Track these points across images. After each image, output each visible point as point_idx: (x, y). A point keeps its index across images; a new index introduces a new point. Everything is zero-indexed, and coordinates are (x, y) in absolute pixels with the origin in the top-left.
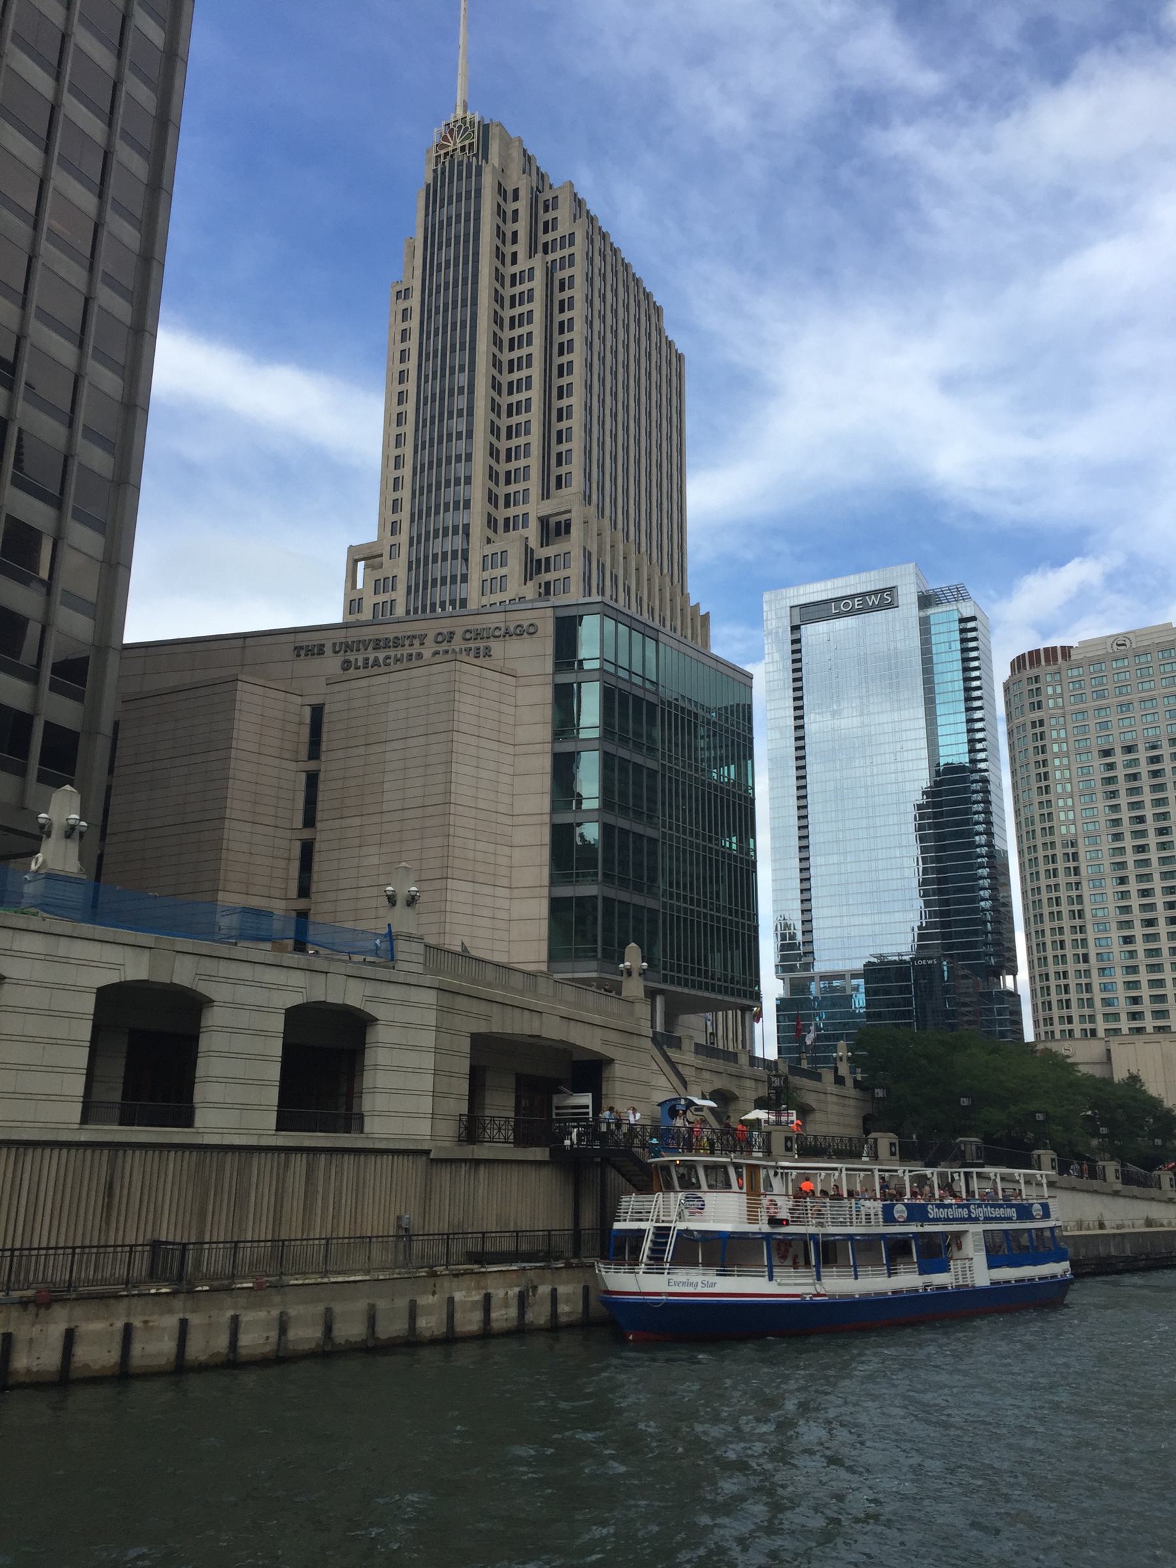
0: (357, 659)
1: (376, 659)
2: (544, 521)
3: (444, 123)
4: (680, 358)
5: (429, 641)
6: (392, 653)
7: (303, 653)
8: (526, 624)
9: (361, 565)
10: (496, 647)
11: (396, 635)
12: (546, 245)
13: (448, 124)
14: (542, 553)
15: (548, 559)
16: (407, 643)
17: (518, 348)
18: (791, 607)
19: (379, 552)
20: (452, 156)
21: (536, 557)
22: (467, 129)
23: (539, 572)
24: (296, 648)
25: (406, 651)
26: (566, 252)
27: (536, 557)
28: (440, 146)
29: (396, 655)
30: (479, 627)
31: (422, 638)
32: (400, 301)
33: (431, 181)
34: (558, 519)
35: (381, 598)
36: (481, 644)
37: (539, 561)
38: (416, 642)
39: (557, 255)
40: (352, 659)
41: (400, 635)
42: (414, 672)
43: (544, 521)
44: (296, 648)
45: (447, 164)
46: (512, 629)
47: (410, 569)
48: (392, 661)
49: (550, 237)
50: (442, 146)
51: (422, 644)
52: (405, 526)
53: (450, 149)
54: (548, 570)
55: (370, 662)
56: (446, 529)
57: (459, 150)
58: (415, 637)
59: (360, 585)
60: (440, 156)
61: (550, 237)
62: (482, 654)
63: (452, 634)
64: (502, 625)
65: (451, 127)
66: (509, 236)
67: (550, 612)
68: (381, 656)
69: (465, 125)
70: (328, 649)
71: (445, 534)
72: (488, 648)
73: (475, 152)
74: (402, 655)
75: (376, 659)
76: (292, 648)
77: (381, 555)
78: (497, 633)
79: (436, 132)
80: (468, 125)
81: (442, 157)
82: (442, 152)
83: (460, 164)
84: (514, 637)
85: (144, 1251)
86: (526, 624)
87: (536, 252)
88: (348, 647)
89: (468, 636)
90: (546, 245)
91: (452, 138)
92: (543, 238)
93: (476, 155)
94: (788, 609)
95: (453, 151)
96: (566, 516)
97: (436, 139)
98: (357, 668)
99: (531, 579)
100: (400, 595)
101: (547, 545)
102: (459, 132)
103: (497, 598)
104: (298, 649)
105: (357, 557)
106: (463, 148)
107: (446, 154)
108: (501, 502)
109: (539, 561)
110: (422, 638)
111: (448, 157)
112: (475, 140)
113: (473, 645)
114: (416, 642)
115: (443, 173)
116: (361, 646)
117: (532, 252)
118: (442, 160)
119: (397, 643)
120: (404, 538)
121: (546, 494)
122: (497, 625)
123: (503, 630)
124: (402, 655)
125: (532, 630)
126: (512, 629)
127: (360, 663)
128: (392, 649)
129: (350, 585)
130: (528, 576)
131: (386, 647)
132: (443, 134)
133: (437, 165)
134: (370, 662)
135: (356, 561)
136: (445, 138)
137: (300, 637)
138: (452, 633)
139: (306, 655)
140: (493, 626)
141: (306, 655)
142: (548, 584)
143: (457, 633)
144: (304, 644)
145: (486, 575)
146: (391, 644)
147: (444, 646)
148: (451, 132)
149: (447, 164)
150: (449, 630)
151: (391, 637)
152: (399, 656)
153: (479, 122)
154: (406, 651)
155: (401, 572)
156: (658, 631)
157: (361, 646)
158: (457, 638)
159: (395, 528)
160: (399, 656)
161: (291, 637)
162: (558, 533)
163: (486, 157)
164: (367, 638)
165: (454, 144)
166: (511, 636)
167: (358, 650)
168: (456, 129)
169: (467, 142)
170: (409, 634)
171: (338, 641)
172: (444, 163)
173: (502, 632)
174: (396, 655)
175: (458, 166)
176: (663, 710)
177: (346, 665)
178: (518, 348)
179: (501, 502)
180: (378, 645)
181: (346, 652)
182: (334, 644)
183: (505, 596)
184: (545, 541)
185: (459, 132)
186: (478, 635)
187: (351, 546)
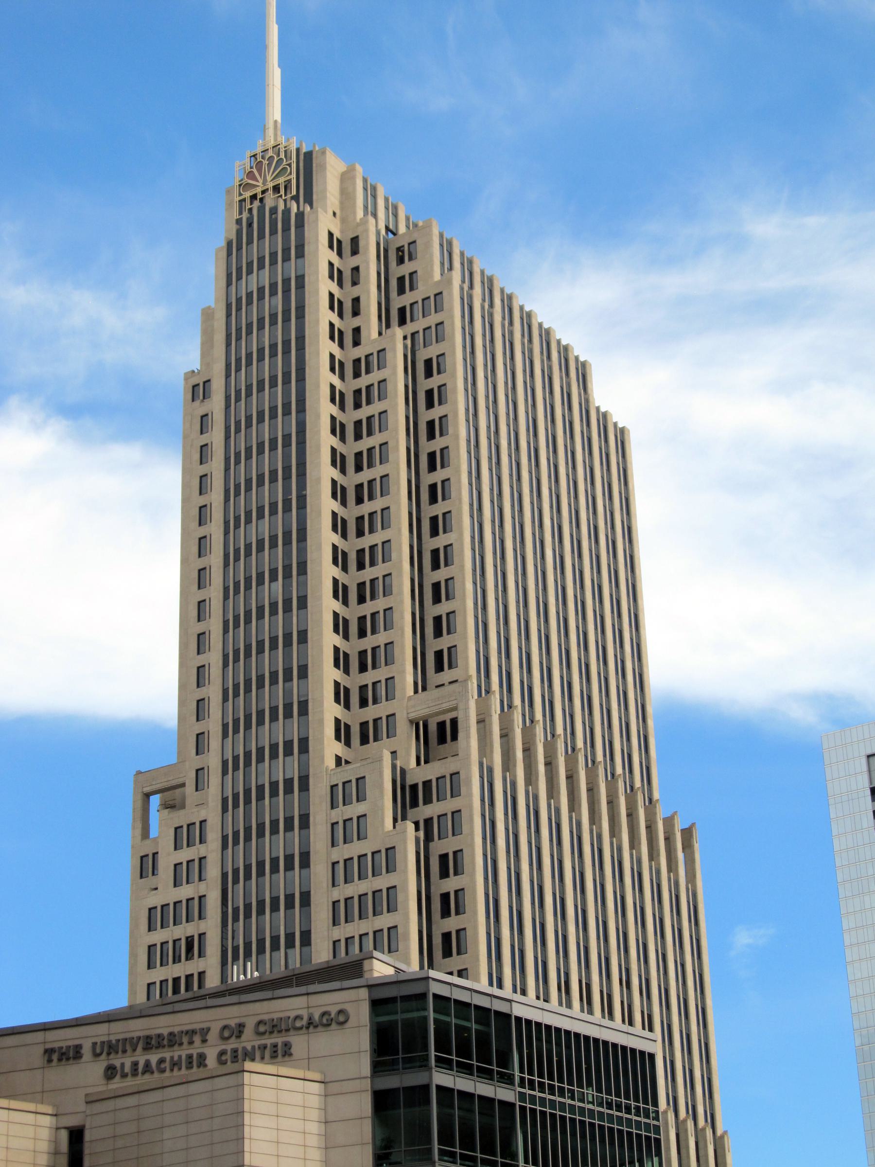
0: (123, 1065)
1: (147, 1064)
2: (420, 727)
3: (248, 154)
4: (622, 435)
5: (213, 1036)
6: (167, 1054)
7: (55, 1057)
8: (333, 1010)
9: (155, 800)
10: (298, 1042)
11: (170, 1030)
12: (402, 311)
13: (255, 156)
14: (418, 775)
15: (427, 784)
16: (185, 1040)
17: (369, 467)
18: (869, 756)
19: (180, 781)
20: (261, 200)
21: (409, 781)
22: (280, 161)
23: (414, 804)
24: (46, 1051)
25: (182, 1052)
26: (432, 319)
27: (409, 781)
30: (276, 1016)
31: (204, 1033)
33: (233, 236)
34: (441, 718)
35: (184, 855)
36: (279, 1040)
37: (414, 787)
38: (197, 1039)
39: (418, 325)
40: (117, 1063)
41: (176, 1030)
42: (194, 1087)
43: (420, 727)
44: (46, 1051)
45: (255, 212)
46: (316, 1017)
47: (225, 809)
48: (167, 1065)
49: (407, 299)
50: (247, 187)
51: (204, 1041)
53: (259, 190)
54: (428, 800)
56: (274, 747)
57: (271, 192)
59: (154, 832)
60: (244, 200)
61: (407, 299)
62: (280, 1052)
63: (241, 1026)
64: (305, 1013)
65: (259, 159)
66: (348, 306)
67: (364, 993)
68: (154, 1058)
69: (278, 155)
71: (274, 755)
72: (287, 1045)
73: (294, 192)
75: (147, 1064)
76: (42, 1051)
77: (183, 785)
78: (298, 1024)
79: (240, 165)
80: (282, 156)
81: (248, 201)
82: (247, 194)
83: (274, 211)
85: (265, 1047)
86: (333, 1010)
87: (388, 326)
88: (111, 1048)
89: (262, 1029)
90: (402, 311)
92: (397, 302)
93: (296, 198)
94: (864, 760)
95: (263, 192)
97: (238, 176)
98: (124, 1076)
99: (404, 818)
100: (212, 849)
101: (426, 762)
102: (269, 165)
103: (355, 849)
104: (49, 1052)
105: (147, 789)
106: (276, 189)
107: (254, 197)
108: (355, 699)
109: (414, 787)
110: (204, 1033)
111: (256, 203)
112: (294, 175)
113: (269, 1041)
114: (197, 1039)
115: (250, 225)
116: (128, 1047)
117: (385, 320)
118: (248, 206)
119: (173, 1040)
120: (213, 760)
121: (422, 685)
122: (299, 1012)
125: (341, 1018)
126: (316, 1017)
127: (127, 1069)
128: (166, 1049)
129: (138, 832)
130: (399, 816)
131: (160, 1046)
132: (248, 169)
133: (241, 213)
135: (147, 796)
137: (52, 1036)
139: (60, 1060)
140: (293, 1014)
141: (60, 1060)
142: (428, 822)
144: (56, 1045)
145: (339, 814)
146: (165, 1042)
147: (230, 1046)
148: (259, 165)
149: (255, 212)
150: (237, 1021)
151: (165, 1032)
152: (176, 1058)
154: (182, 1052)
155: (212, 814)
156: (510, 1001)
157: (128, 1047)
158: (248, 1032)
159: (200, 743)
160: (176, 1058)
161: (40, 1036)
162: (442, 740)
163: (309, 200)
166: (316, 1027)
167: (124, 1051)
168: (266, 162)
169: (281, 180)
170: (185, 1028)
171: (98, 1040)
172: (250, 210)
173: (304, 1022)
174: (172, 1058)
176: (523, 1109)
177: (110, 1072)
178: (369, 467)
180: (150, 1043)
181: (109, 1054)
182: (95, 1044)
183: (365, 847)
184: (425, 758)
185: (269, 165)
186: (275, 1027)
187: (139, 773)
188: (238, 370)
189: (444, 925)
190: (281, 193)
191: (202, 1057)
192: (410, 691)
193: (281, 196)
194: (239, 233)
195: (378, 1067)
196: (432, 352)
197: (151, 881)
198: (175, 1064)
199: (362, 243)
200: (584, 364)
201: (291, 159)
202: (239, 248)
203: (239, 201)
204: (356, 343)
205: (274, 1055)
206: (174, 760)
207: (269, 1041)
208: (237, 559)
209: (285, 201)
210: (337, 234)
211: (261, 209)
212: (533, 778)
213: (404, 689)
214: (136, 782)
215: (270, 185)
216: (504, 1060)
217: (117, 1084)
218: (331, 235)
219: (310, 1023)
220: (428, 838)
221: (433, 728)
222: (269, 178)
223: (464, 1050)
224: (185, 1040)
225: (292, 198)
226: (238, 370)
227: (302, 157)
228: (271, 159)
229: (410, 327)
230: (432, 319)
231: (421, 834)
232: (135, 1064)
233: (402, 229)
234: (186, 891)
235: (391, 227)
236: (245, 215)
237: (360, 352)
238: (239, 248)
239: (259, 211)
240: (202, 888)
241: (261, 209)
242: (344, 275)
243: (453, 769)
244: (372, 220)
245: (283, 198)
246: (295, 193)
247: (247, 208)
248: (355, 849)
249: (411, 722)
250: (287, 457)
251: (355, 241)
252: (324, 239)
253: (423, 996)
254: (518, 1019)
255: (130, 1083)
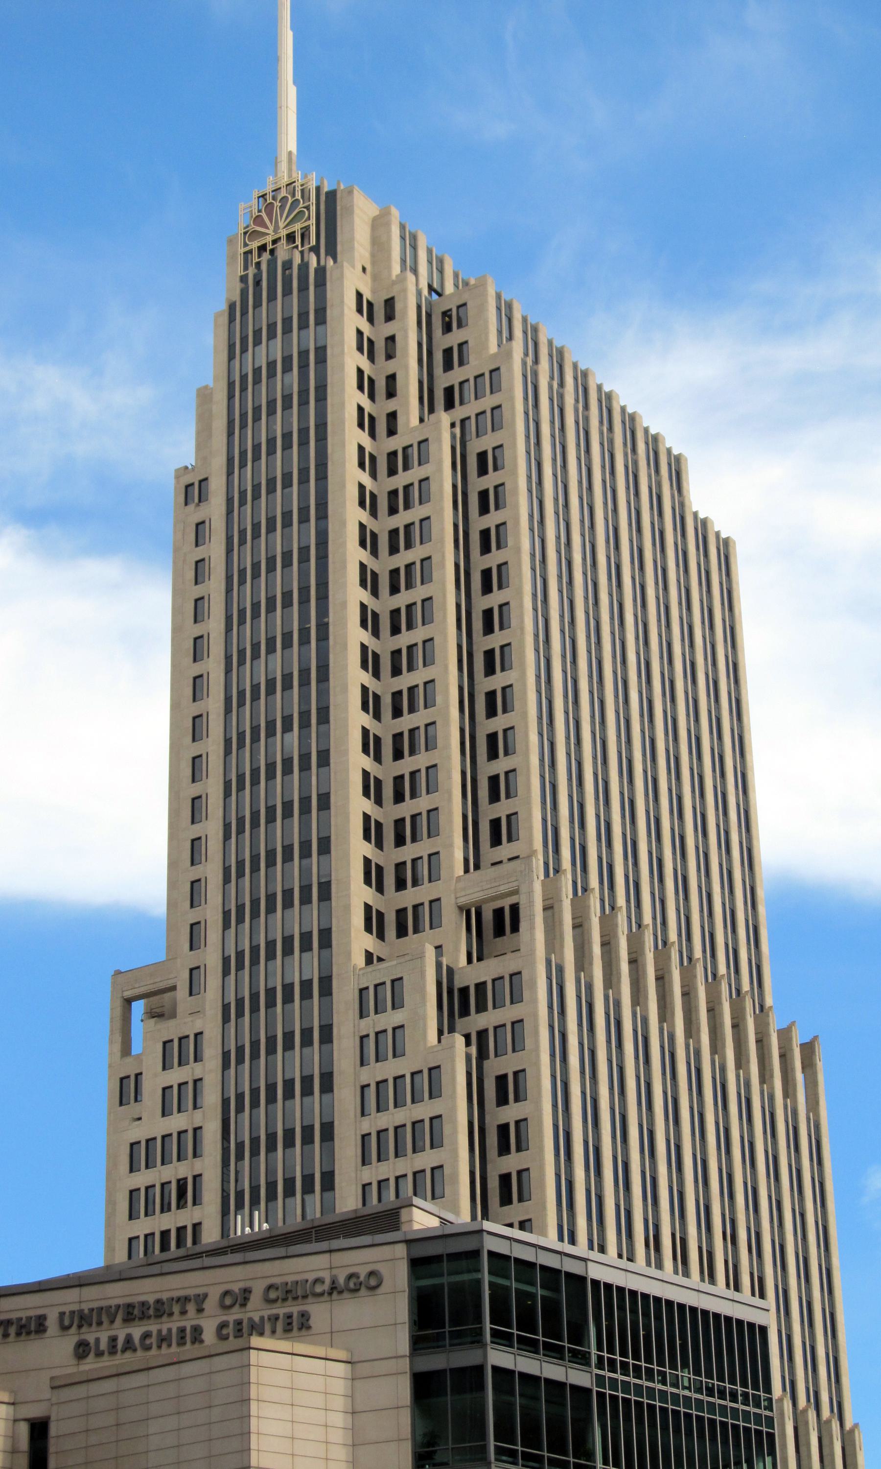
0: (97, 1340)
1: (129, 1340)
3: (256, 194)
4: (726, 547)
5: (211, 1304)
7: (12, 1330)
8: (363, 1272)
9: (138, 1008)
10: (319, 1312)
11: (158, 1296)
13: (263, 196)
15: (481, 987)
16: (176, 1309)
19: (170, 983)
20: (272, 252)
21: (458, 984)
22: (295, 203)
23: (465, 1012)
25: (172, 1325)
26: (487, 402)
27: (458, 984)
28: (250, 234)
29: (160, 1331)
30: (290, 1279)
31: (200, 1300)
32: (191, 507)
33: (237, 298)
34: (498, 904)
35: (176, 1076)
36: (294, 1309)
38: (191, 1308)
39: (470, 409)
40: (91, 1338)
41: (165, 1296)
42: (187, 1369)
45: (264, 267)
46: (341, 1280)
47: (226, 1019)
48: (153, 1340)
50: (254, 235)
51: (200, 1310)
52: (214, 934)
53: (269, 239)
54: (481, 1007)
55: (120, 1345)
57: (284, 241)
58: (187, 1299)
59: (137, 1047)
60: (251, 252)
63: (247, 1291)
64: (326, 1276)
65: (269, 200)
67: (401, 1251)
68: (137, 1332)
69: (294, 195)
70: (52, 1323)
73: (313, 242)
74: (170, 1330)
75: (129, 1340)
77: (173, 988)
78: (319, 1289)
80: (298, 196)
82: (255, 245)
83: (287, 265)
84: (346, 1295)
86: (363, 1272)
88: (83, 1319)
89: (273, 1295)
90: (449, 392)
91: (271, 222)
92: (443, 380)
93: (315, 249)
95: (275, 242)
96: (513, 900)
97: (242, 222)
98: (99, 1354)
99: (452, 1030)
101: (480, 959)
102: (282, 208)
103: (389, 1069)
105: (128, 994)
106: (291, 237)
107: (262, 248)
108: (390, 880)
109: (464, 991)
110: (200, 1300)
111: (266, 256)
112: (313, 221)
113: (281, 1310)
114: (191, 1308)
115: (258, 283)
116: (104, 1318)
117: (427, 401)
118: (256, 260)
119: (161, 1309)
120: (211, 957)
122: (321, 1274)
123: (328, 1282)
124: (170, 1330)
125: (373, 1282)
126: (341, 1280)
127: (103, 1345)
128: (152, 1321)
129: (117, 1047)
131: (144, 1316)
132: (255, 213)
133: (246, 268)
134: (120, 1345)
135: (128, 1002)
136: (258, 220)
138: (247, 1291)
139: (18, 1334)
140: (311, 1277)
141: (18, 1334)
142: (482, 1035)
143: (254, 1291)
144: (14, 1316)
148: (269, 208)
149: (264, 267)
150: (242, 1285)
151: (151, 1299)
152: (164, 1332)
153: (318, 189)
154: (172, 1325)
157: (104, 1318)
158: (256, 1299)
160: (164, 1332)
162: (499, 931)
163: (332, 251)
164: (113, 1302)
165: (276, 228)
166: (341, 1292)
167: (100, 1323)
168: (277, 204)
169: (297, 227)
171: (67, 1309)
172: (258, 264)
173: (326, 1286)
174: (160, 1331)
175: (284, 270)
176: (601, 1396)
177: (82, 1350)
178: (407, 588)
179: (390, 880)
181: (80, 1327)
185: (282, 208)
187: (118, 973)
188: (243, 465)
189: (502, 1164)
190: (297, 243)
191: (197, 1331)
192: (459, 870)
193: (297, 247)
194: (244, 293)
195: (418, 1344)
196: (487, 443)
197: (133, 1109)
198: (164, 1340)
199: (398, 306)
200: (678, 459)
201: (309, 201)
202: (244, 313)
203: (245, 253)
204: (392, 431)
205: (288, 1328)
206: (162, 956)
207: (281, 1310)
208: (241, 703)
209: (302, 253)
210: (367, 295)
211: (272, 263)
212: (614, 980)
213: (451, 867)
214: (114, 984)
215: (283, 233)
216: (578, 1335)
217: (90, 1365)
218: (359, 295)
219: (334, 1288)
220: (482, 1055)
221: (488, 916)
222: (281, 224)
223: (527, 1322)
224: (176, 1309)
225: (311, 249)
226: (243, 465)
227: (323, 198)
228: (284, 200)
229: (459, 412)
230: (487, 402)
231: (473, 1049)
232: (113, 1340)
233: (449, 289)
234: (177, 1122)
235: (435, 286)
236: (251, 271)
237: (396, 443)
238: (244, 313)
239: (269, 265)
240: (198, 1118)
241: (272, 263)
242: (376, 308)
243: (513, 969)
244: (411, 277)
245: (300, 249)
246: (314, 243)
247: (254, 262)
248: (389, 1069)
249: (461, 908)
250: (304, 575)
251: (390, 303)
252: (350, 301)
253: (475, 1254)
254: (596, 1283)
255: (107, 1363)
